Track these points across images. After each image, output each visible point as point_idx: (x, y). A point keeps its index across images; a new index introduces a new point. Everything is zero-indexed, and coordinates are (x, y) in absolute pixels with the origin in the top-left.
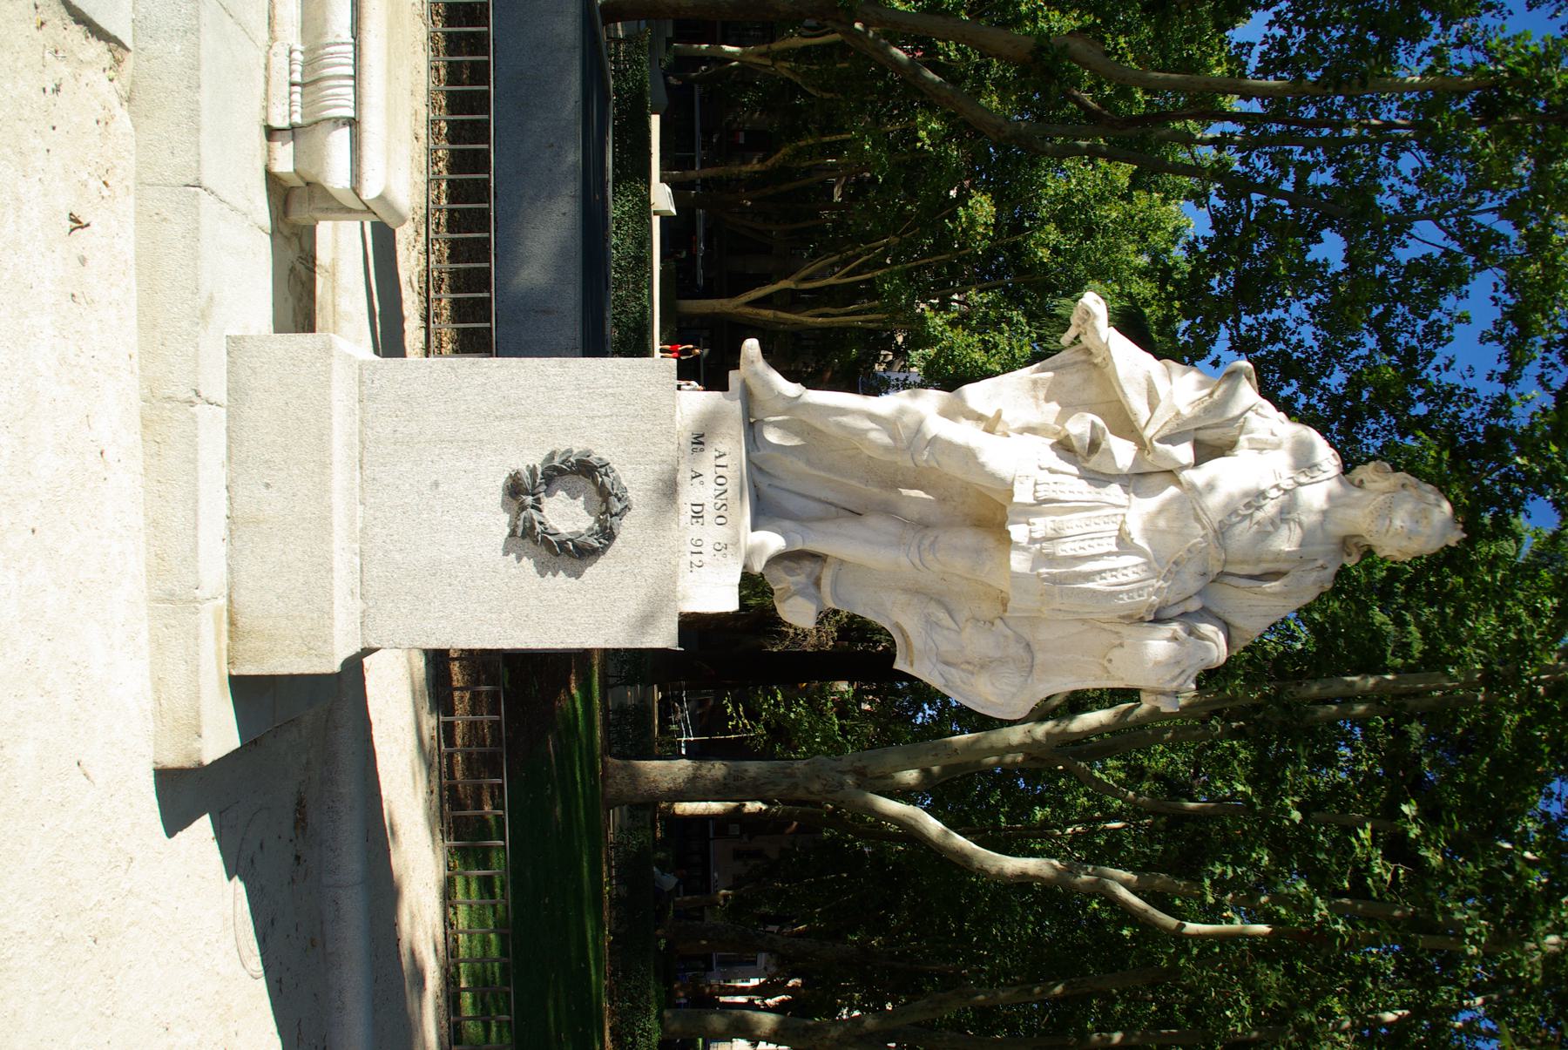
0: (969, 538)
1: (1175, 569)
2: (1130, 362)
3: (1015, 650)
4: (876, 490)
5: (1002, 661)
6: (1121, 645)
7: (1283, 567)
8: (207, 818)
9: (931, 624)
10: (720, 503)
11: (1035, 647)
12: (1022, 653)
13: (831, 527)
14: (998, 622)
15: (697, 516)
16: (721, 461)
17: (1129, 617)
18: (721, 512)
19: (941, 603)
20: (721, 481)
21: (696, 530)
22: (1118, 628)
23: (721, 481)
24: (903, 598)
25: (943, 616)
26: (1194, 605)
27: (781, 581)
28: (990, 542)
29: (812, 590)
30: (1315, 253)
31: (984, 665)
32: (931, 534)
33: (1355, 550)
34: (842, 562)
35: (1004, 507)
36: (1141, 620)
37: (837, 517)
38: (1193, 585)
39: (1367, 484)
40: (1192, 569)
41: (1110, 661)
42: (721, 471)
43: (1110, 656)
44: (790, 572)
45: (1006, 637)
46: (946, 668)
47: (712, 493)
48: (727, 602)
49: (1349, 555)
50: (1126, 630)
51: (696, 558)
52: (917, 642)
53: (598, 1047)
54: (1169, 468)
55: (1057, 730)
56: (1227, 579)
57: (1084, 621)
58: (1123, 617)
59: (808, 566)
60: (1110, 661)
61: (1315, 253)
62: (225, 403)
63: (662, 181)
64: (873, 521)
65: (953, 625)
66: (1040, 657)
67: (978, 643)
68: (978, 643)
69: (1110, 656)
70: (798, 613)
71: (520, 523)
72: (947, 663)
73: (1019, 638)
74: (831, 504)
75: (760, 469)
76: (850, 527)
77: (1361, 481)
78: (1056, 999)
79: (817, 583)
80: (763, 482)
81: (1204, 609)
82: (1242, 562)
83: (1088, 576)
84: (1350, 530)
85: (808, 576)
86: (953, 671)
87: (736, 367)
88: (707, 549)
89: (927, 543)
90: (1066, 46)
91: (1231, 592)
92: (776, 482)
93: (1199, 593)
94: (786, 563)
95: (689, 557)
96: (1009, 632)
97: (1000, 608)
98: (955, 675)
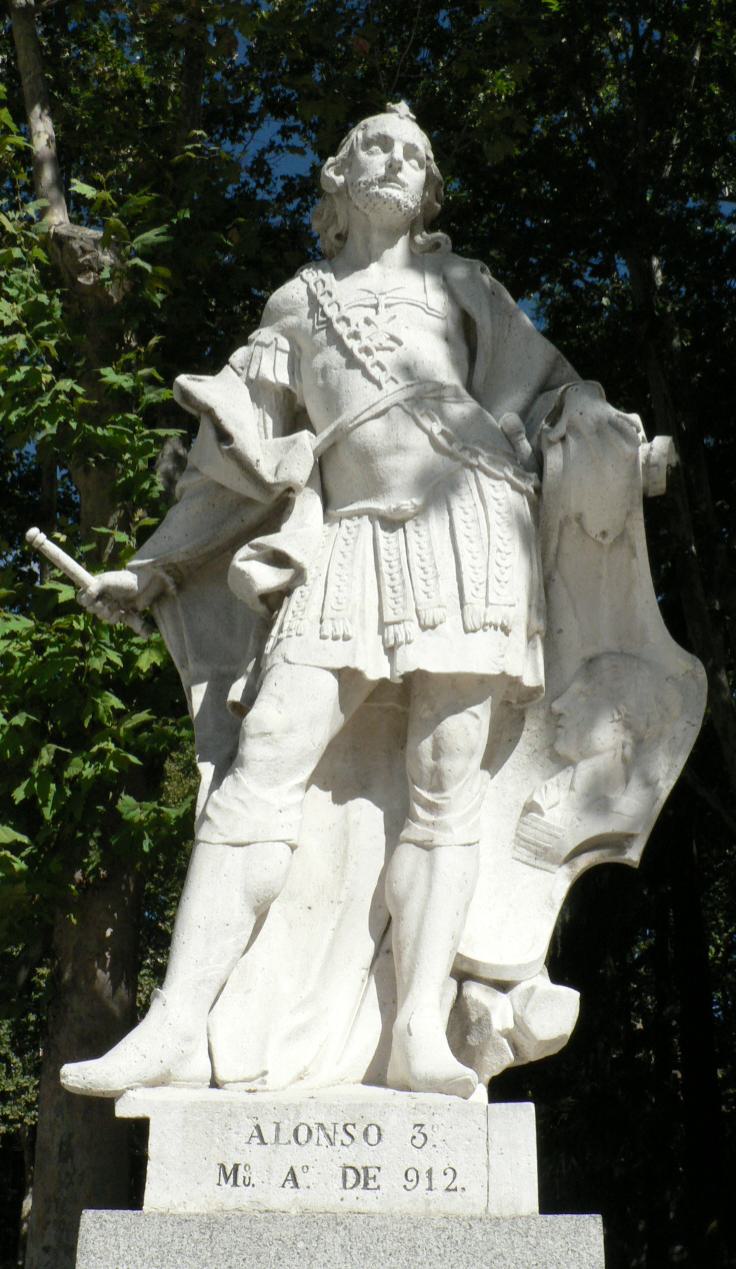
6: (579, 518)
8: (488, 702)
10: (342, 1136)
15: (363, 1177)
16: (269, 1133)
18: (357, 1133)
20: (303, 1134)
21: (389, 1181)
30: (396, 47)
42: (286, 1134)
47: (324, 1151)
48: (523, 1117)
51: (440, 1182)
60: (604, 534)
61: (396, 47)
62: (288, 349)
63: (16, 841)
70: (553, 1014)
78: (654, 313)
88: (422, 1160)
90: (43, 544)
95: (439, 1193)
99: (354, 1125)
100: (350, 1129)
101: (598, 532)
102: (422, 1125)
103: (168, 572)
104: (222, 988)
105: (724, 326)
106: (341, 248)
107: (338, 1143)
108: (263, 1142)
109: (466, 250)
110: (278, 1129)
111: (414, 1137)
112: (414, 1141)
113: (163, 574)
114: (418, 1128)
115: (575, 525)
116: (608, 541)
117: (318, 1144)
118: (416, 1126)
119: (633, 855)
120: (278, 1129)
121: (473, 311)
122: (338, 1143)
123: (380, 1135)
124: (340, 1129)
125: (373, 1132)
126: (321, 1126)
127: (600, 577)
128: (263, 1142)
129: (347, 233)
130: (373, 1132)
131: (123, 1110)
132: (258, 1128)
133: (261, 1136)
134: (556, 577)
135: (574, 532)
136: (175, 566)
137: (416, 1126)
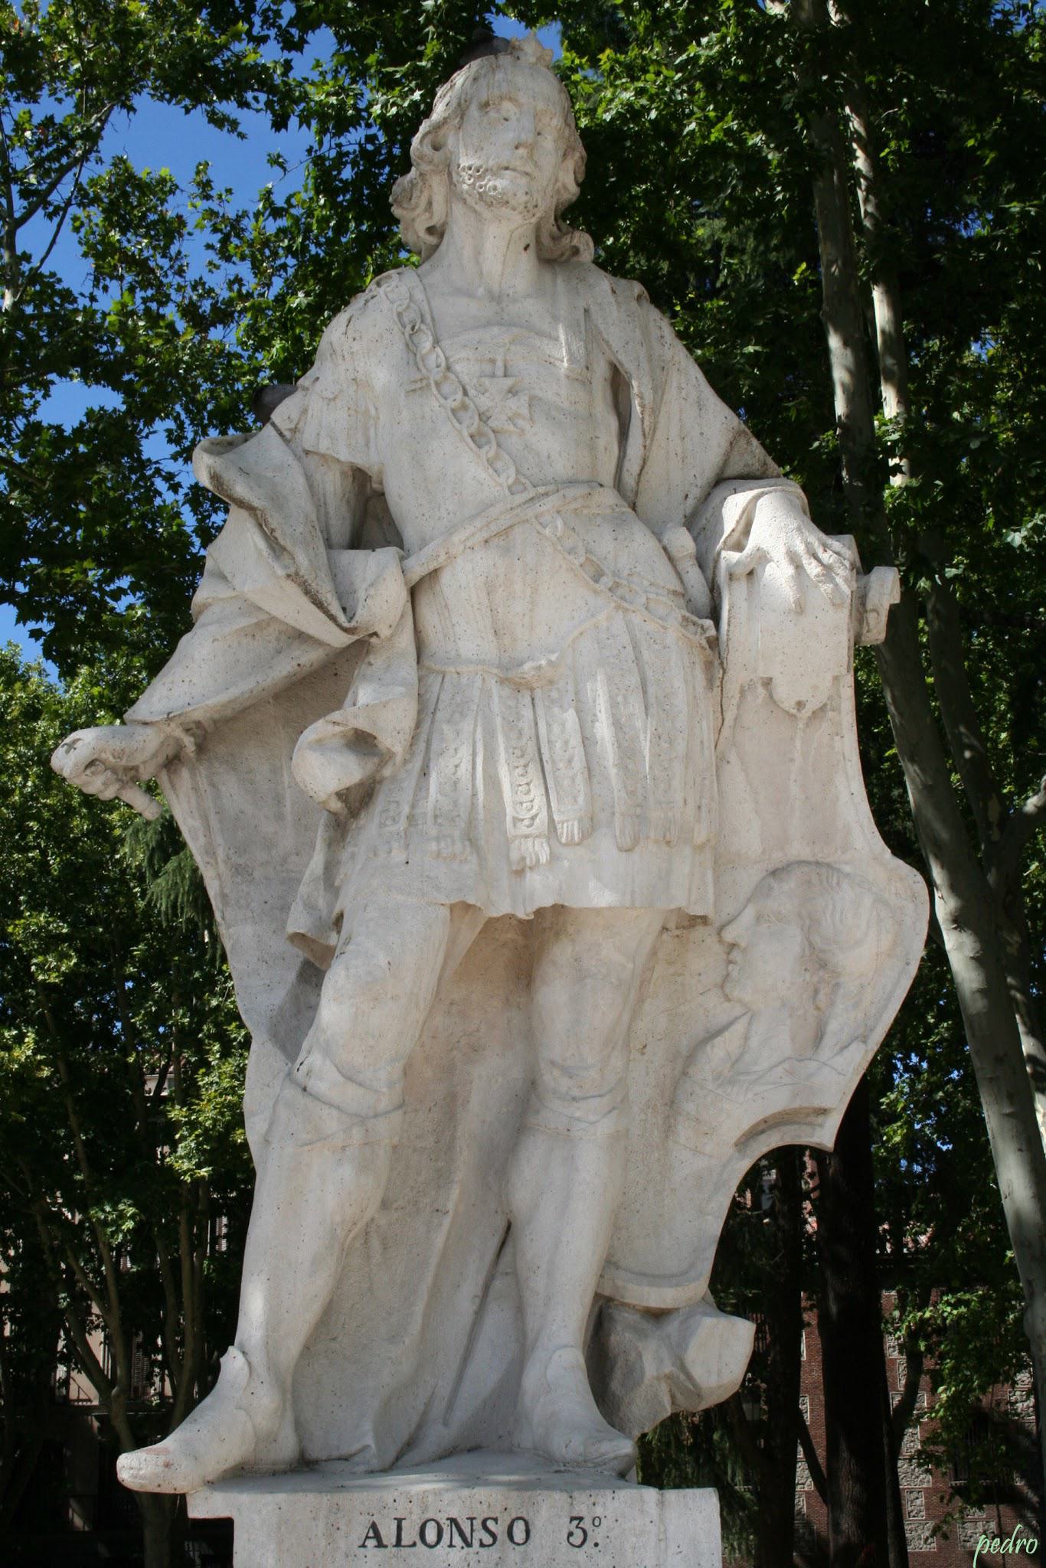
0: (554, 994)
1: (607, 581)
2: (196, 677)
3: (785, 897)
4: (455, 1192)
5: (810, 924)
6: (768, 683)
7: (601, 371)
9: (735, 1073)
10: (480, 1534)
11: (777, 858)
12: (790, 884)
13: (538, 1283)
14: (729, 935)
16: (388, 1533)
17: (708, 665)
19: (691, 1058)
20: (431, 1535)
22: (732, 688)
23: (431, 1535)
24: (684, 1132)
25: (718, 1052)
26: (683, 542)
27: (650, 1402)
28: (562, 953)
29: (672, 1327)
31: (818, 962)
32: (550, 1078)
33: (566, 241)
34: (609, 1264)
35: (491, 923)
36: (714, 643)
37: (514, 1274)
38: (642, 542)
39: (436, 219)
40: (605, 544)
41: (800, 705)
43: (789, 705)
44: (633, 1374)
45: (758, 919)
46: (829, 1041)
49: (576, 251)
50: (737, 676)
52: (777, 1101)
53: (806, 5)
54: (404, 595)
55: (1023, 1010)
56: (629, 480)
57: (721, 760)
58: (710, 682)
59: (621, 1337)
60: (800, 705)
64: (521, 1196)
65: (739, 1027)
66: (798, 849)
67: (774, 966)
68: (774, 966)
69: (789, 705)
70: (721, 1352)
71: (222, 867)
72: (819, 1037)
73: (761, 891)
74: (487, 1288)
75: (410, 1444)
76: (534, 1245)
77: (431, 230)
79: (657, 1316)
80: (437, 1436)
81: (690, 522)
82: (592, 448)
83: (627, 751)
84: (526, 263)
85: (642, 1334)
86: (833, 1026)
87: (178, 1502)
89: (564, 1084)
91: (654, 470)
92: (439, 1407)
93: (658, 535)
94: (615, 1385)
96: (749, 914)
97: (700, 931)
98: (840, 1023)
99: (496, 1520)
100: (490, 1524)
101: (793, 703)
102: (581, 1519)
103: (187, 730)
104: (503, 1244)
105: (943, 491)
106: (437, 246)
107: (476, 1543)
108: (380, 1545)
109: (890, 1086)
110: (399, 1528)
111: (571, 1534)
112: (572, 1539)
113: (179, 733)
114: (575, 1522)
115: (761, 691)
116: (806, 713)
117: (472, 1519)
118: (572, 1519)
119: (826, 1135)
120: (399, 1528)
121: (628, 365)
122: (476, 1543)
123: (528, 1532)
124: (477, 1524)
125: (519, 1527)
126: (453, 1521)
127: (792, 760)
128: (380, 1545)
129: (445, 224)
130: (519, 1527)
131: (198, 1510)
132: (374, 1526)
133: (377, 1536)
134: (733, 757)
135: (760, 700)
136: (198, 724)
137: (572, 1519)
